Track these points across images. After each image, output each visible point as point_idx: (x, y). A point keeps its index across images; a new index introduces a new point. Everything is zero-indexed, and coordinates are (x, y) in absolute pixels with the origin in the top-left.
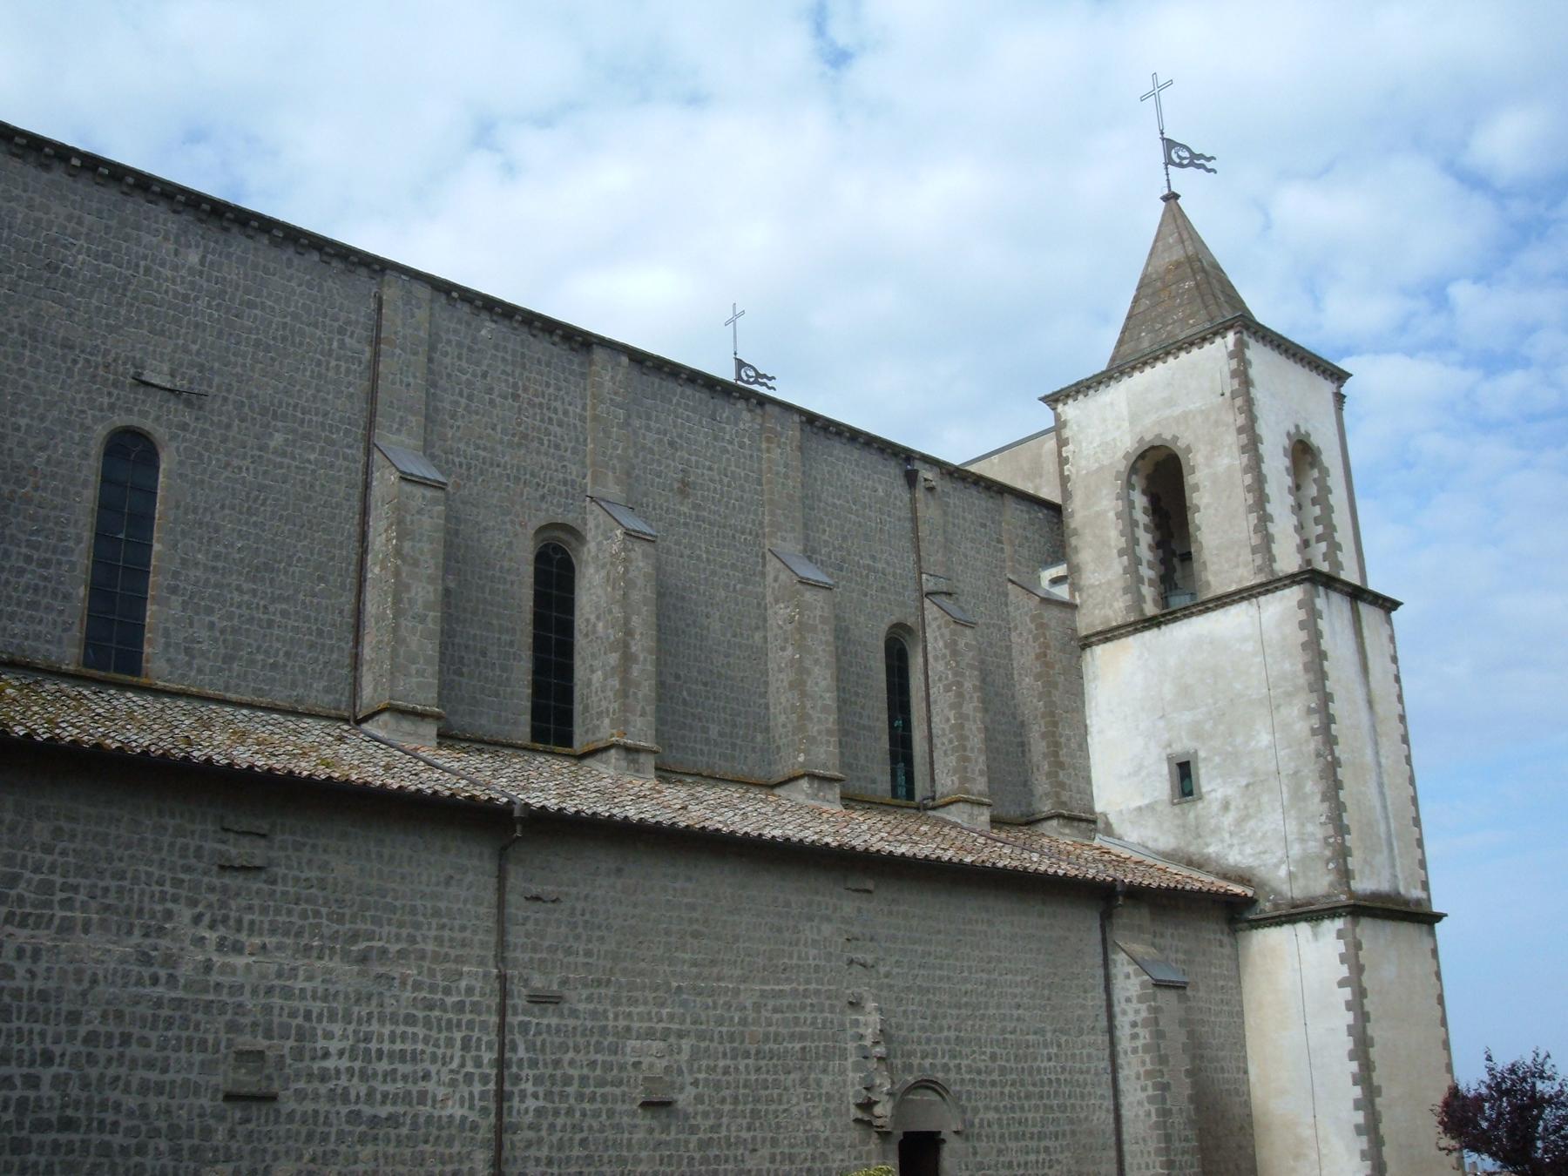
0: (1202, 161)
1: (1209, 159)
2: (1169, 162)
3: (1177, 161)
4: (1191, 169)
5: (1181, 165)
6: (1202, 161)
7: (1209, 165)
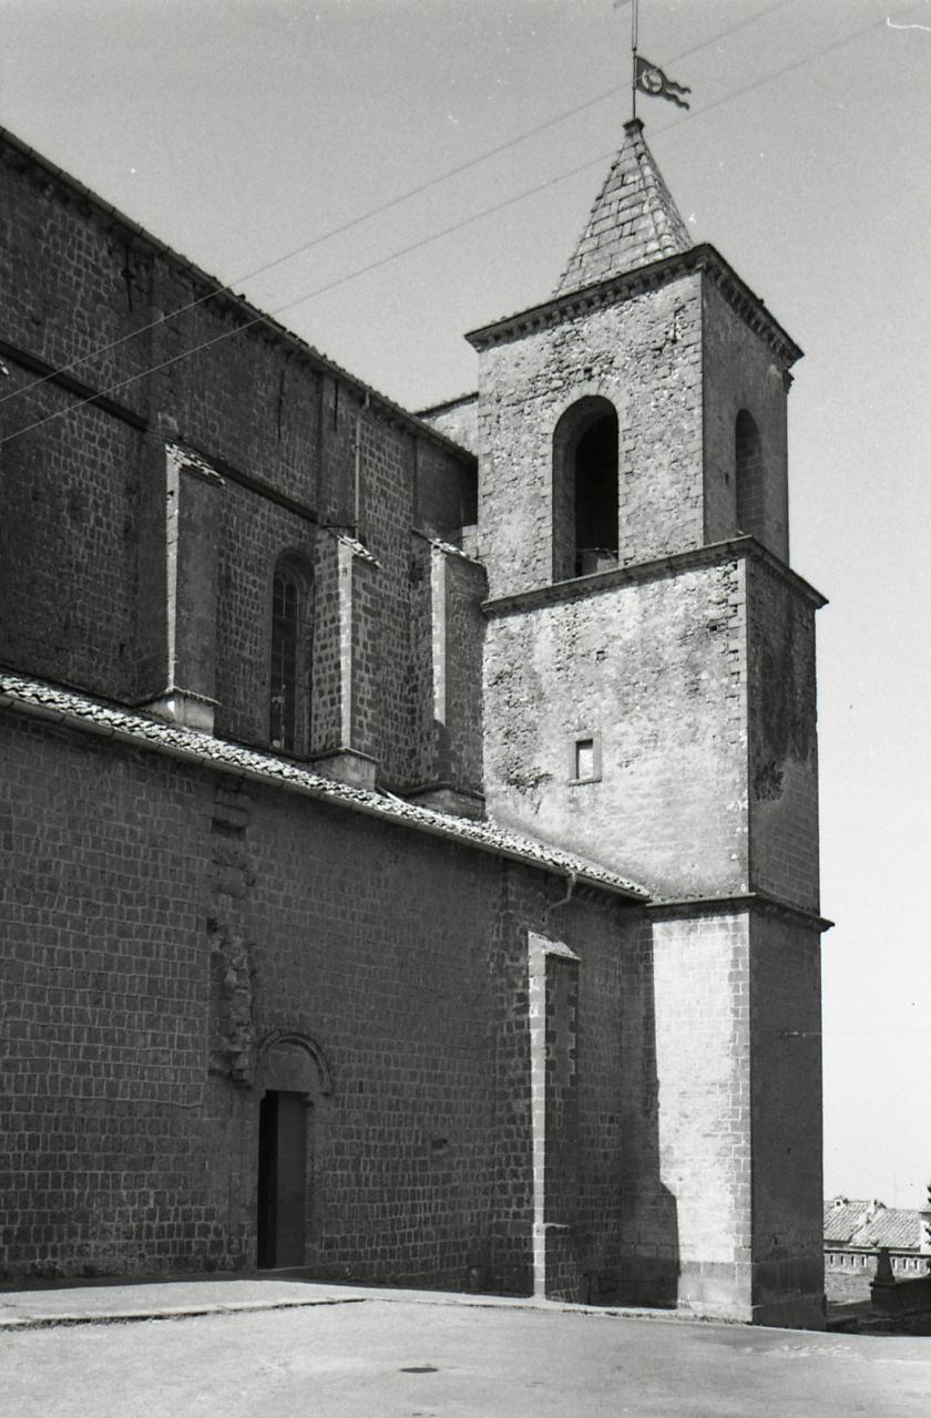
0: (675, 92)
1: (685, 90)
2: (638, 85)
3: (647, 86)
4: (661, 101)
5: (650, 92)
6: (675, 92)
7: (682, 97)
